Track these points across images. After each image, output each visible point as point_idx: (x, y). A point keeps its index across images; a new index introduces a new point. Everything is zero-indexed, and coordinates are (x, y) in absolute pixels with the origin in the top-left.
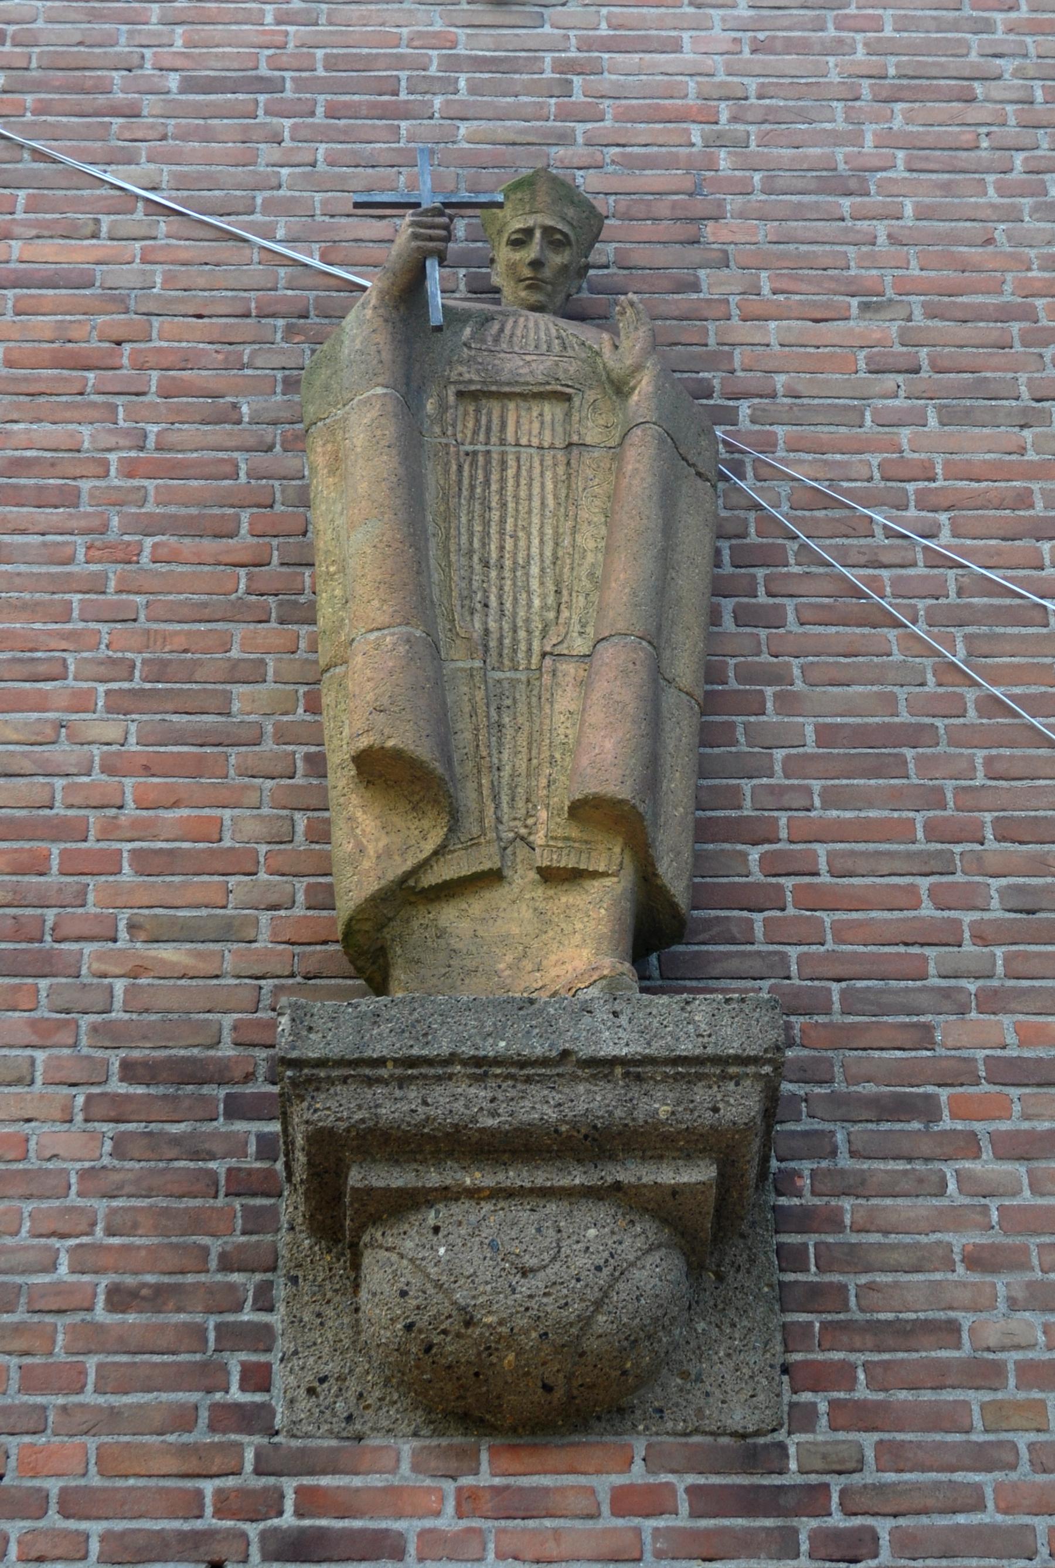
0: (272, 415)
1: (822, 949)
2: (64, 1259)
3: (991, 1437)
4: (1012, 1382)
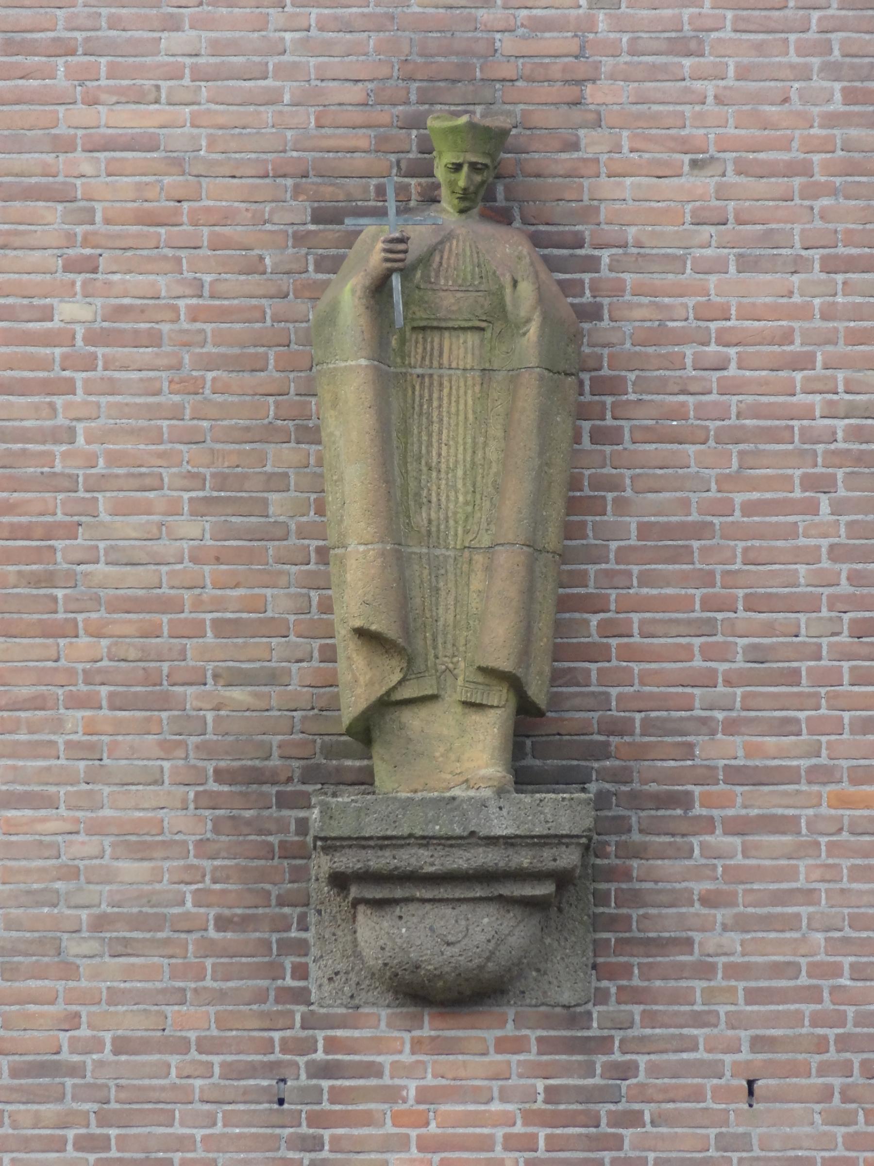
0: (287, 267)
1: (632, 689)
2: (189, 898)
3: (706, 1008)
4: (720, 975)
